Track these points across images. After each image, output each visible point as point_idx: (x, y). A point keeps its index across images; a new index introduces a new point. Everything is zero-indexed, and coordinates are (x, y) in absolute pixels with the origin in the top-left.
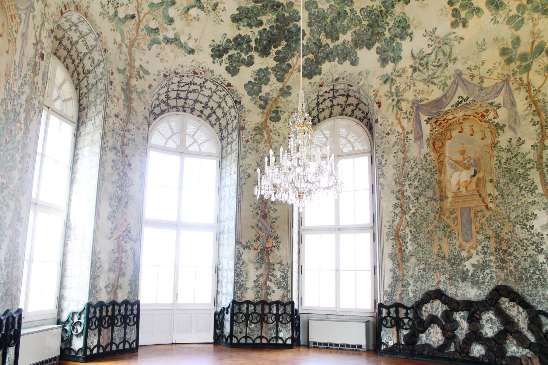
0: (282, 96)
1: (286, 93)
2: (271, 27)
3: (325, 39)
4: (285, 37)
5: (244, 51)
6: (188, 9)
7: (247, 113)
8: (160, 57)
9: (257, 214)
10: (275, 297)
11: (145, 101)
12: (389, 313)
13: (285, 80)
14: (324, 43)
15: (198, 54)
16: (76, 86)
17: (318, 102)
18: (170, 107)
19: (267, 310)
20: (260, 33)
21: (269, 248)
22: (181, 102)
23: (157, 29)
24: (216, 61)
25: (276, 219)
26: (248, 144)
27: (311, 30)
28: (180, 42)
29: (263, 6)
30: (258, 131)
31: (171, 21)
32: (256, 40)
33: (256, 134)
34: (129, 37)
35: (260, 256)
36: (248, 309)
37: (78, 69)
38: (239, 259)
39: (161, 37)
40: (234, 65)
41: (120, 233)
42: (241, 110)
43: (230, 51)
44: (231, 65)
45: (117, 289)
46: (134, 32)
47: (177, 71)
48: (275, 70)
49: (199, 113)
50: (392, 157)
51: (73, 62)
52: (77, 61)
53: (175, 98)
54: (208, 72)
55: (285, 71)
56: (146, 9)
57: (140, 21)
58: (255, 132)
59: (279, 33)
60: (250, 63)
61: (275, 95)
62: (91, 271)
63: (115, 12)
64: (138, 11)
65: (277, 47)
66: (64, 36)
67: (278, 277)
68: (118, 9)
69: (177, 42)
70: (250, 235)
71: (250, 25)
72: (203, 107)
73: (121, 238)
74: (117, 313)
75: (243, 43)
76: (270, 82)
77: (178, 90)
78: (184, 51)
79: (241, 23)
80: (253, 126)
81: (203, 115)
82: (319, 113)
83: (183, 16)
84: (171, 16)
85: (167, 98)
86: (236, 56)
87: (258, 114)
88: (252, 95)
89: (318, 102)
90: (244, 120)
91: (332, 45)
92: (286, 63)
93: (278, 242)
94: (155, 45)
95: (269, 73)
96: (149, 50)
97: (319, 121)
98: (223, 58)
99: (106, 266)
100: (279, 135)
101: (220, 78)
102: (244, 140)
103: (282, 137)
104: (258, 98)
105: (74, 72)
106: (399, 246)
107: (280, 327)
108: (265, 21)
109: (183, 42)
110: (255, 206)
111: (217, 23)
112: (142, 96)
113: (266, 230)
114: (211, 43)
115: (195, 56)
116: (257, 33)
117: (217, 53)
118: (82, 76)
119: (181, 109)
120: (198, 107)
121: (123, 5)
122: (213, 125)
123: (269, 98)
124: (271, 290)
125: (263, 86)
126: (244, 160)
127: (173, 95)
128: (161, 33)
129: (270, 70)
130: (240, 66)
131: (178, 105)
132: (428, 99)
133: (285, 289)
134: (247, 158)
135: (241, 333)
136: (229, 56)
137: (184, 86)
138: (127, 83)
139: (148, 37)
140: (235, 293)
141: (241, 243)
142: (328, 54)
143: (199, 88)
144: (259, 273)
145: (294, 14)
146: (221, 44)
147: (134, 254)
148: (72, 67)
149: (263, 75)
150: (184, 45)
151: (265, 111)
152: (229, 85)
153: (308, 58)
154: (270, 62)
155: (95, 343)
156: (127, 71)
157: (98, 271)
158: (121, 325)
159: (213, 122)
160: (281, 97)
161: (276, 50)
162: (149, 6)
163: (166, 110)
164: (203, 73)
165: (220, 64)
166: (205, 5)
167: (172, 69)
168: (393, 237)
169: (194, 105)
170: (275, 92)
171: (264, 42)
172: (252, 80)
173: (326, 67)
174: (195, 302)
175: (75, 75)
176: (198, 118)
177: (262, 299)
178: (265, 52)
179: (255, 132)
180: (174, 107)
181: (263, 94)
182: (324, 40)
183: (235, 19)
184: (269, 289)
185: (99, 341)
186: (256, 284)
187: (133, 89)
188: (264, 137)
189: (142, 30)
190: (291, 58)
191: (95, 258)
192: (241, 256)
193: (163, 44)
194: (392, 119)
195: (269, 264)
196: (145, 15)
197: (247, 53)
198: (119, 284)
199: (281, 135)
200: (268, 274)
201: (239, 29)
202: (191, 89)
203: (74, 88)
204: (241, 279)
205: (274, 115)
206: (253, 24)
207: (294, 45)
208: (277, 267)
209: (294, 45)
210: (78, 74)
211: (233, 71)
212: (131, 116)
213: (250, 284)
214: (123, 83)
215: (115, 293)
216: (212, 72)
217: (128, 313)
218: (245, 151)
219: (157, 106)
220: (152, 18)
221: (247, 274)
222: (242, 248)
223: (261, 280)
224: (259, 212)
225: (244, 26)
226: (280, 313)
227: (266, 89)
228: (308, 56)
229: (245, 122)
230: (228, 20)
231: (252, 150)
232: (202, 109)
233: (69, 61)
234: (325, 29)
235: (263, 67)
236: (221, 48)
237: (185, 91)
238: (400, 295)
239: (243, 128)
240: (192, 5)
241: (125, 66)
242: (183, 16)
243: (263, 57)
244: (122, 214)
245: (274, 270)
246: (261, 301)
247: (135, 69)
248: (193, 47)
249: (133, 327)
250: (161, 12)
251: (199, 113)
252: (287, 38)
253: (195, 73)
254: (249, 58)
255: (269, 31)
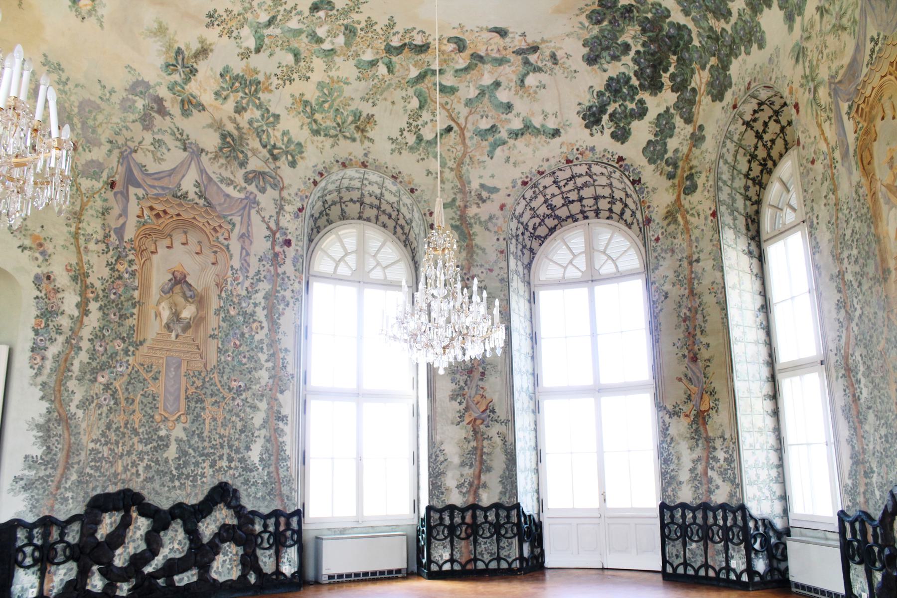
0: (694, 146)
1: (699, 138)
2: (644, 45)
3: (717, 23)
4: (669, 49)
5: (628, 98)
6: (522, 81)
7: (651, 193)
8: (512, 160)
9: (684, 356)
10: (720, 497)
11: (496, 229)
12: (265, 526)
13: (695, 119)
14: (719, 31)
15: (566, 132)
16: (404, 242)
17: (757, 132)
18: (561, 221)
19: (458, 520)
20: (635, 61)
21: (705, 411)
22: (575, 208)
23: (493, 127)
24: (594, 131)
25: (709, 360)
26: (659, 244)
27: (693, 19)
28: (535, 127)
29: (610, 22)
30: (670, 219)
31: (509, 107)
32: (636, 73)
33: (669, 224)
34: (453, 156)
35: (694, 426)
36: (684, 516)
37: (399, 222)
38: (665, 434)
39: (504, 134)
40: (622, 125)
41: (475, 415)
42: (643, 193)
43: (608, 107)
44: (618, 126)
45: (478, 488)
46: (460, 147)
47: (541, 170)
48: (678, 107)
49: (607, 214)
50: (823, 207)
51: (390, 217)
52: (394, 215)
53: (563, 205)
54: (587, 152)
55: (692, 102)
56: (464, 111)
57: (462, 129)
58: (667, 222)
59: (659, 46)
60: (642, 112)
61: (685, 149)
62: (429, 467)
63: (417, 137)
64: (453, 120)
65: (668, 70)
66: (362, 195)
67: (722, 461)
68: (421, 132)
69: (530, 130)
70: (677, 392)
71: (615, 58)
72: (609, 203)
73: (478, 422)
74: (711, 521)
75: (621, 88)
76: (676, 130)
77: (562, 193)
78: (544, 137)
79: (603, 61)
80: (662, 211)
81: (614, 215)
82: (769, 150)
83: (521, 93)
84: (505, 101)
85: (552, 209)
86: (620, 110)
87: (667, 190)
88: (654, 163)
89: (757, 132)
90: (649, 207)
91: (728, 28)
92: (689, 88)
93: (716, 400)
94: (499, 149)
95: (672, 116)
96: (492, 158)
97: (775, 165)
98: (603, 123)
99: (456, 460)
100: (699, 215)
101: (606, 154)
102: (653, 238)
103: (702, 217)
104: (663, 164)
105: (395, 227)
106: (852, 390)
107: (731, 551)
108: (630, 41)
109: (538, 126)
110: (679, 344)
111: (572, 77)
112: (490, 225)
113: (699, 382)
114: (578, 108)
115: (563, 138)
116: (631, 64)
117: (592, 119)
118: (407, 228)
119: (580, 216)
120: (603, 204)
121: (426, 123)
122: (629, 226)
123: (678, 158)
124: (714, 484)
125: (668, 140)
126: (656, 272)
127: (558, 201)
128: (501, 129)
129: (672, 111)
130: (630, 123)
131: (573, 213)
132: (842, 66)
133: (733, 482)
134: (660, 268)
135: (677, 556)
136: (611, 115)
137: (566, 184)
138: (461, 216)
139: (485, 143)
140: (664, 490)
141: (665, 408)
142: (730, 46)
143: (587, 178)
144: (695, 456)
145: (657, 10)
146: (592, 103)
147: (504, 441)
148: (391, 224)
149: (664, 122)
150: (542, 130)
151: (676, 181)
152: (621, 159)
153: (712, 66)
154: (668, 98)
155: (446, 556)
156: (459, 200)
157: (441, 467)
158: (492, 536)
159: (629, 220)
160: (694, 149)
161: (668, 75)
162: (466, 105)
163: (556, 226)
164: (580, 156)
165: (602, 132)
166: (540, 64)
167: (533, 170)
168: (843, 372)
169: (597, 203)
170: (685, 143)
171: (648, 71)
172: (652, 138)
173: (736, 68)
174: (576, 506)
175: (399, 229)
176: (608, 221)
177: (703, 500)
178: (655, 87)
179: (667, 222)
180: (568, 217)
181: (670, 154)
182: (719, 25)
183: (592, 60)
184: (711, 483)
185: (452, 555)
186: (693, 475)
187: (473, 221)
188: (679, 225)
189: (471, 138)
190: (692, 77)
191: (434, 450)
192: (667, 429)
193: (511, 142)
194: (814, 131)
195: (708, 440)
196: (466, 118)
197: (633, 99)
198: (482, 482)
199: (701, 213)
200: (708, 457)
201: (605, 71)
202: (579, 185)
203: (402, 245)
204: (671, 468)
205: (688, 183)
206: (618, 54)
207: (687, 55)
208: (718, 443)
209: (687, 55)
210: (402, 227)
211: (621, 136)
212: (475, 257)
213: (684, 476)
214: (453, 219)
215: (476, 495)
216: (593, 149)
217: (502, 522)
218: (656, 257)
219: (540, 225)
220: (479, 117)
221: (679, 458)
222: (668, 416)
223: (700, 468)
224: (686, 353)
225: (608, 63)
226: (729, 525)
227: (672, 144)
228: (711, 63)
229: (651, 209)
230: (583, 66)
231: (666, 252)
232: (609, 206)
233: (383, 218)
234: (707, 7)
235: (662, 110)
236: (594, 109)
237: (574, 190)
238: (864, 493)
239: (648, 221)
240: (523, 73)
241: (454, 196)
242: (521, 93)
243: (656, 94)
244: (477, 390)
245: (715, 449)
246: (700, 505)
247: (473, 193)
248: (555, 127)
249: (513, 540)
250: (489, 104)
251: (607, 214)
252: (673, 49)
253: (568, 161)
254: (639, 105)
255: (644, 52)
